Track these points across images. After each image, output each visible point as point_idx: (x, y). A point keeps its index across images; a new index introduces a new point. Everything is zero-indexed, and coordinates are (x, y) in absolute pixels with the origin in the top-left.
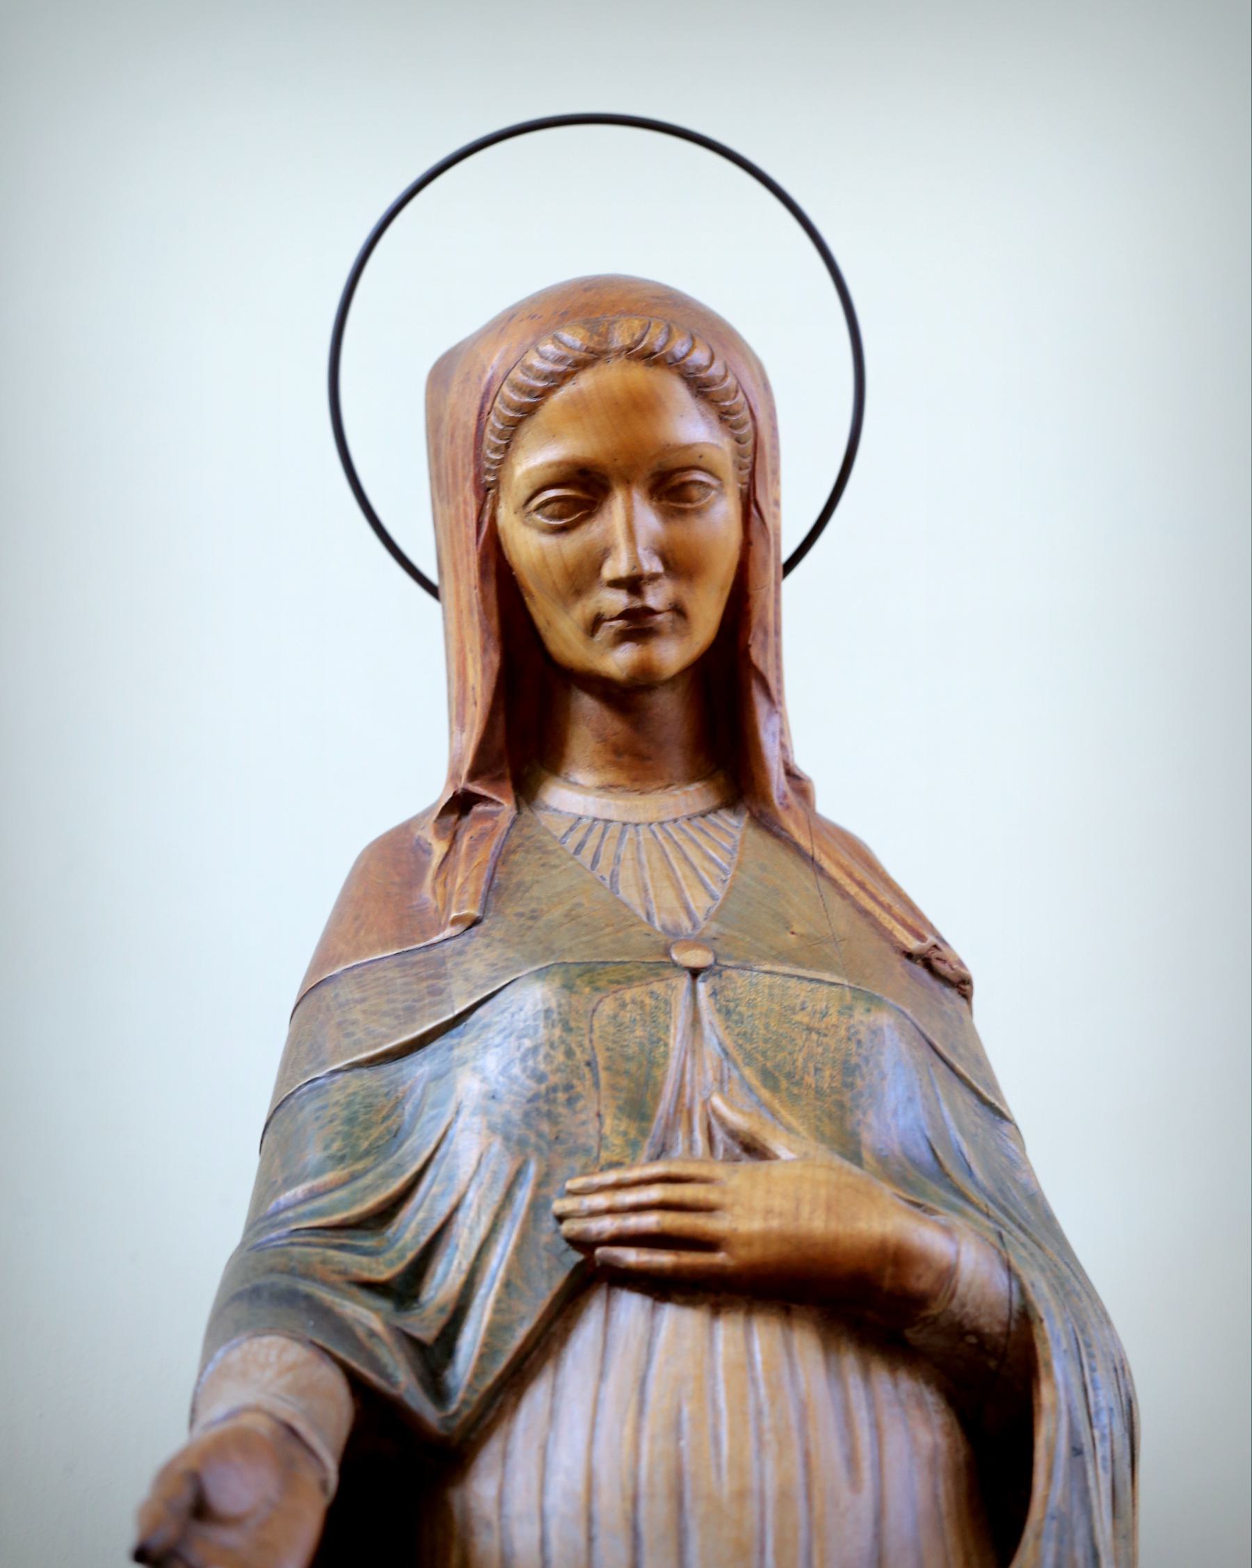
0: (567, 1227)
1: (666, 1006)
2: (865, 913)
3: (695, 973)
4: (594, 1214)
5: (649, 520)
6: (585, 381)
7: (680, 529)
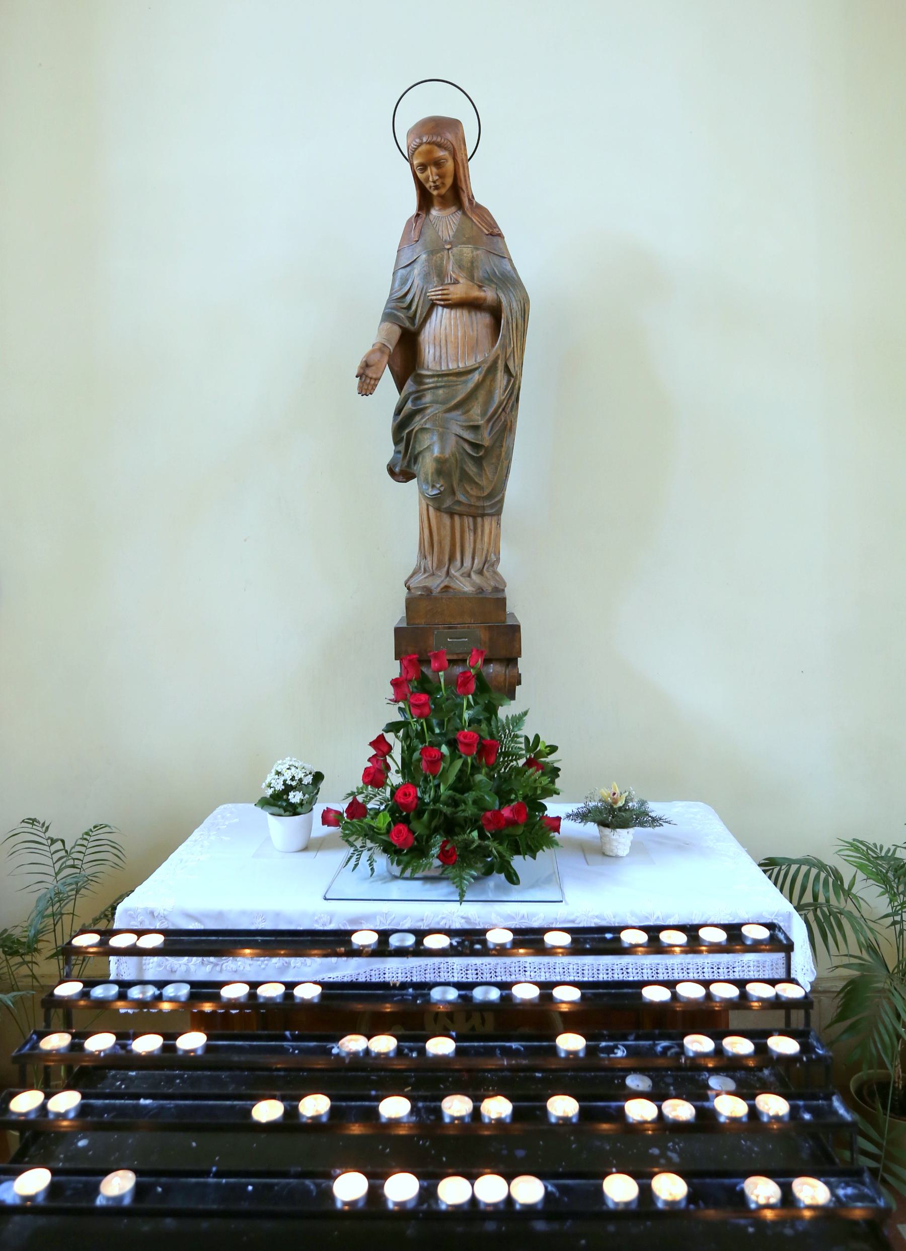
0: (429, 298)
1: (443, 256)
2: (479, 228)
3: (448, 249)
4: (432, 296)
5: (434, 170)
6: (420, 149)
7: (440, 170)
